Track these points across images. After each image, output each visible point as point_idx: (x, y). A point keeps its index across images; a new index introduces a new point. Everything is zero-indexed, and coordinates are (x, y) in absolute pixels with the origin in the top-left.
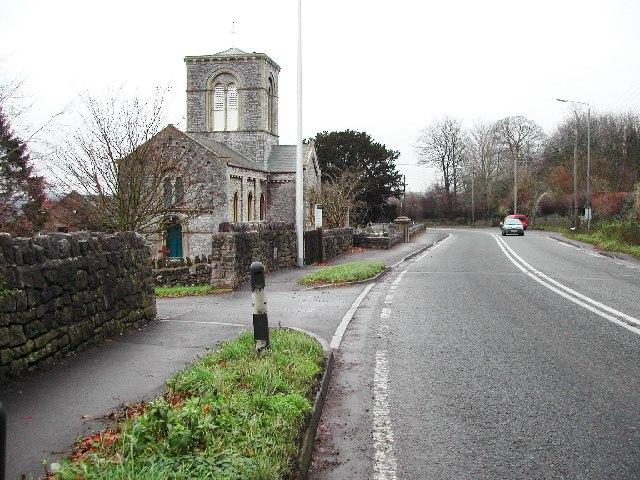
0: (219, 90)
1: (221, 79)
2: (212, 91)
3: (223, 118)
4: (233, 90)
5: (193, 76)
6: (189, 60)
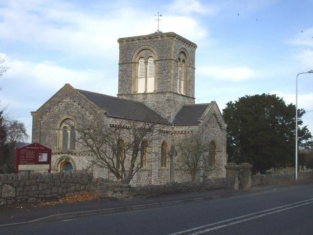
6: (121, 41)
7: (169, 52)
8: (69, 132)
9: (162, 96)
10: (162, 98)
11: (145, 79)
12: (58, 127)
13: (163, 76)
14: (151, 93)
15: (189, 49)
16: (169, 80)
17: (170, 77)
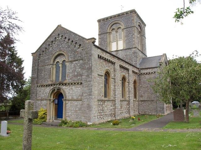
5: (101, 27)
6: (99, 21)
7: (133, 22)
8: (60, 65)
9: (129, 51)
10: (129, 52)
11: (116, 42)
12: (52, 62)
13: (128, 39)
14: (121, 50)
15: (142, 25)
16: (134, 40)
17: (134, 38)
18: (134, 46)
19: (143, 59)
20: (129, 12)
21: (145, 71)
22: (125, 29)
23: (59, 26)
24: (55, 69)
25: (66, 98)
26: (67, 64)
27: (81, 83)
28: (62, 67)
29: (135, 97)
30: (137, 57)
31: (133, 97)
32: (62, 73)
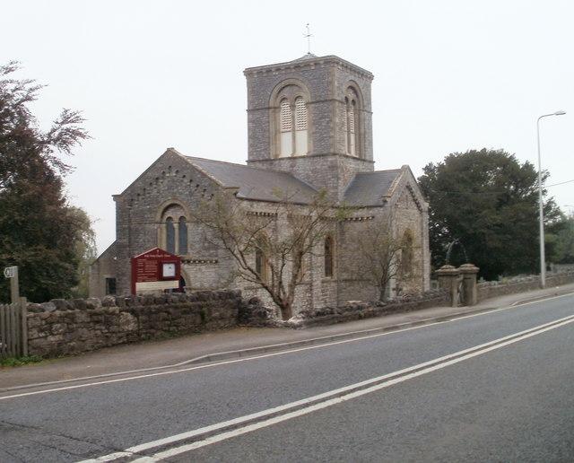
0: (285, 107)
1: (286, 93)
2: (277, 108)
3: (298, 148)
4: (300, 104)
5: (254, 91)
6: (249, 73)
7: (330, 88)
8: (176, 225)
9: (321, 160)
10: (321, 164)
11: (290, 134)
12: (158, 218)
14: (303, 157)
15: (361, 83)
18: (332, 151)
19: (359, 177)
20: (322, 62)
21: (356, 214)
22: (313, 103)
23: (170, 152)
24: (165, 231)
25: (190, 285)
26: (190, 226)
27: (217, 262)
28: (179, 229)
29: (329, 271)
30: (338, 179)
31: (322, 270)
32: (180, 239)
